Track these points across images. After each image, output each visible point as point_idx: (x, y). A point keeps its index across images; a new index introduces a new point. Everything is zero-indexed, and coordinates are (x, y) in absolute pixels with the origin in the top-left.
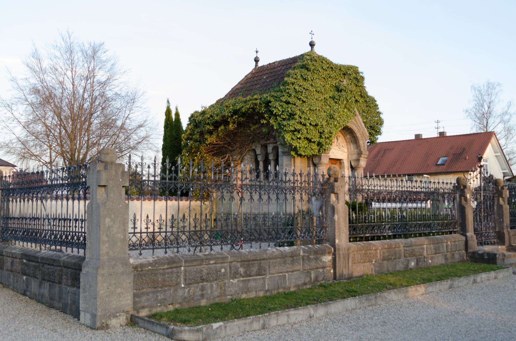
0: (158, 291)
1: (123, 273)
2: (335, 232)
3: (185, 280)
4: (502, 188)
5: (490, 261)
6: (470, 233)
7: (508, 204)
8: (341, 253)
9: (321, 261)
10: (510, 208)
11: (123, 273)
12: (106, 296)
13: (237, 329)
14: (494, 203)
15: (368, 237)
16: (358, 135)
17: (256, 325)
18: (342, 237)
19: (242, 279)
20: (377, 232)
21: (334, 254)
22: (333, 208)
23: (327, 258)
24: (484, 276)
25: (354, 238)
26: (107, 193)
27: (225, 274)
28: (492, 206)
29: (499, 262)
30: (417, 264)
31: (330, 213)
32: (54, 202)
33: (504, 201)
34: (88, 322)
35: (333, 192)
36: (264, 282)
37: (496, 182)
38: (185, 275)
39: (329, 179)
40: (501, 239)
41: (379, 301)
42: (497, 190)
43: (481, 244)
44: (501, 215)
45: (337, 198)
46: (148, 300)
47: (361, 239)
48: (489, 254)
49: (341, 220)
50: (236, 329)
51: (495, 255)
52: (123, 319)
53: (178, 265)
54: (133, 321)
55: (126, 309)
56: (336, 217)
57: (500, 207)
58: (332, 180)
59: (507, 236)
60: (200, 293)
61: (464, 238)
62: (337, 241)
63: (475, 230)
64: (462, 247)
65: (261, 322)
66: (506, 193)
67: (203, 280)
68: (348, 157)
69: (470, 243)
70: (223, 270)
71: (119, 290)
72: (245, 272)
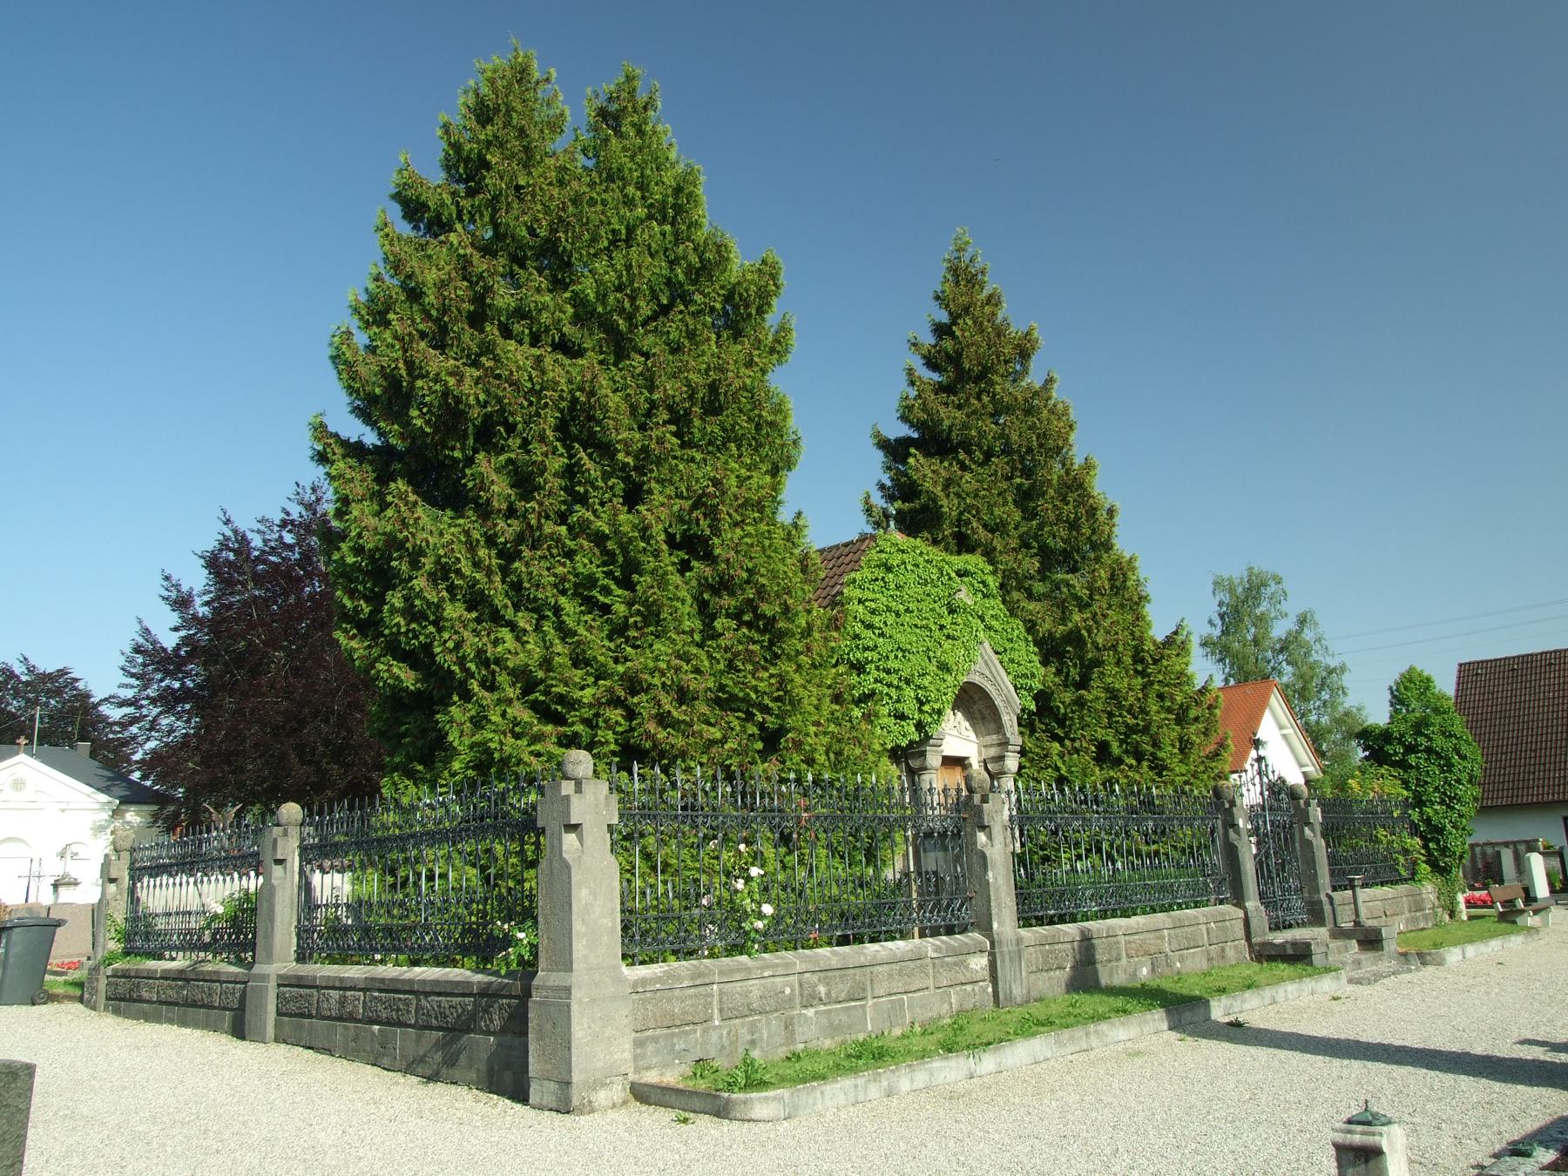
0: (673, 1035)
1: (614, 998)
2: (989, 906)
3: (721, 1010)
4: (1307, 804)
5: (1299, 956)
6: (1252, 904)
7: (1323, 836)
8: (1005, 950)
9: (967, 967)
10: (1328, 846)
11: (614, 998)
12: (587, 1044)
13: (842, 1097)
14: (1292, 835)
15: (1052, 916)
16: (998, 702)
17: (874, 1091)
18: (1004, 919)
19: (822, 1008)
20: (1068, 906)
21: (992, 955)
22: (983, 856)
23: (979, 963)
24: (1291, 988)
25: (1025, 920)
26: (581, 840)
27: (791, 999)
28: (1289, 841)
29: (1316, 959)
30: (1153, 970)
31: (977, 868)
32: (338, 876)
33: (1313, 830)
34: (549, 1100)
35: (983, 828)
36: (865, 1014)
37: (1293, 794)
38: (721, 1002)
39: (970, 798)
40: (1317, 917)
41: (1094, 1042)
42: (1297, 808)
43: (1277, 926)
44: (1311, 862)
45: (990, 837)
46: (657, 1052)
47: (1041, 921)
48: (1294, 944)
49: (1001, 881)
50: (842, 1100)
51: (1308, 945)
52: (618, 1091)
53: (707, 980)
54: (643, 1094)
55: (622, 1070)
56: (990, 874)
57: (1308, 844)
58: (977, 798)
59: (1327, 908)
60: (749, 1037)
61: (1241, 914)
62: (995, 925)
63: (1262, 896)
64: (1241, 933)
65: (885, 1084)
66: (1316, 814)
67: (753, 1012)
68: (980, 753)
69: (1254, 923)
70: (788, 991)
71: (608, 1032)
72: (828, 994)
